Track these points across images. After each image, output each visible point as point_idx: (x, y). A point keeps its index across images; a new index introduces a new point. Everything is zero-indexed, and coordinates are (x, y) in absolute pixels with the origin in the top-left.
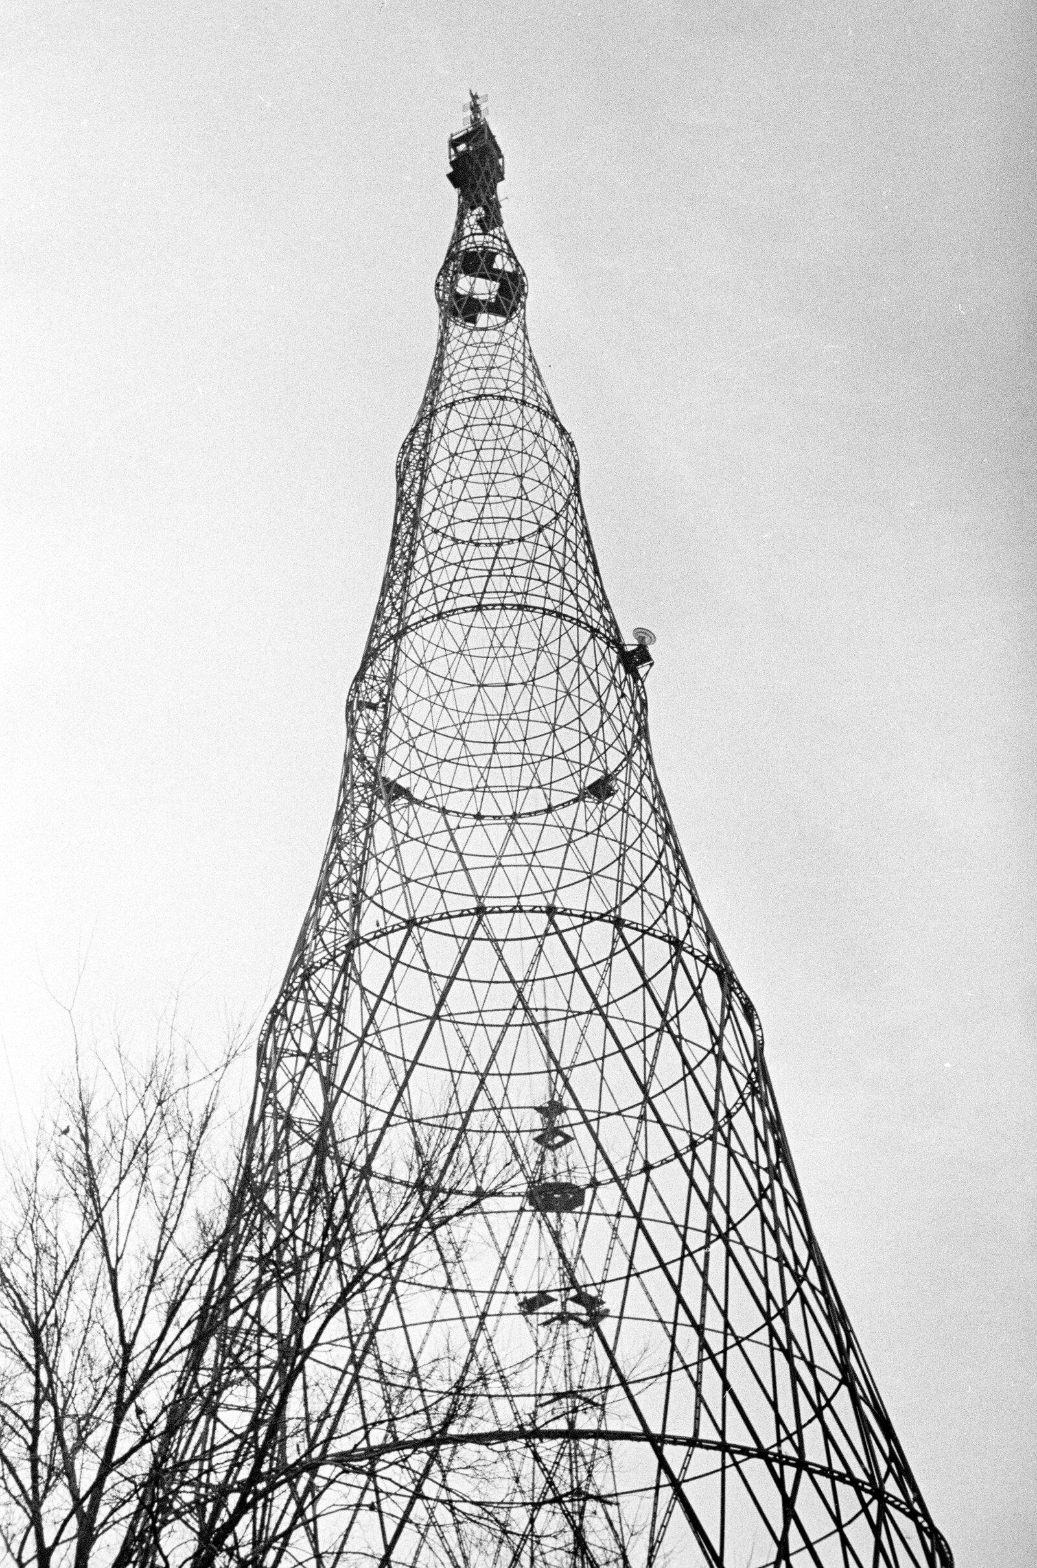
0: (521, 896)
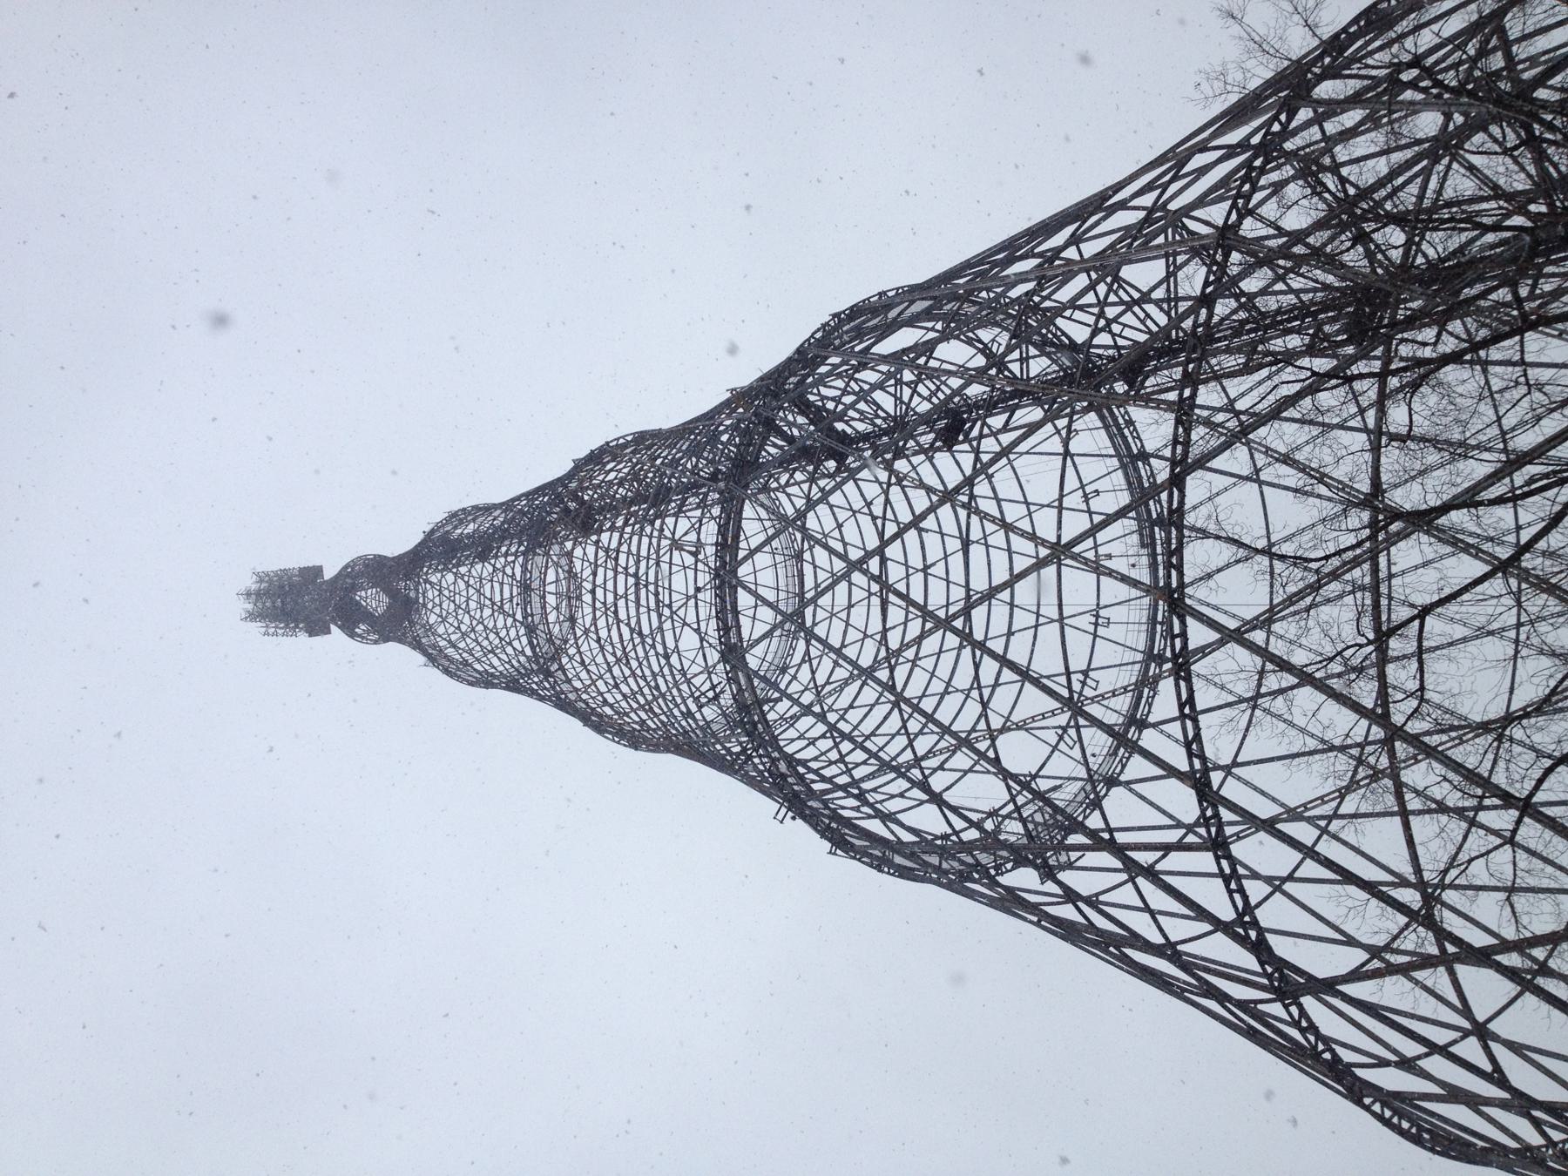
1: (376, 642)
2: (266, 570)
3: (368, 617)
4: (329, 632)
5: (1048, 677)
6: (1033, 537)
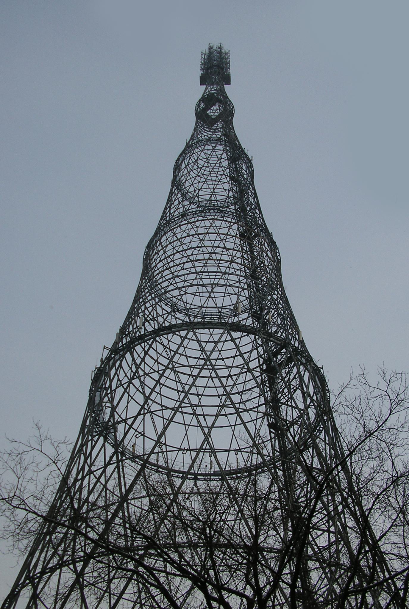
0: (221, 350)
1: (196, 110)
2: (231, 57)
3: (207, 108)
4: (201, 84)
5: (164, 425)
6: (213, 350)
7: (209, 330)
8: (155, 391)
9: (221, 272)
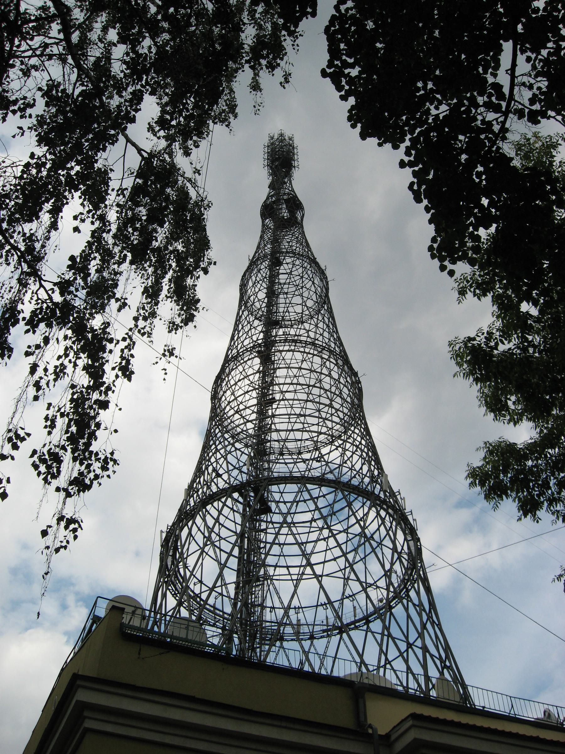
0: (283, 492)
7: (234, 583)
8: (317, 625)
9: (295, 414)
